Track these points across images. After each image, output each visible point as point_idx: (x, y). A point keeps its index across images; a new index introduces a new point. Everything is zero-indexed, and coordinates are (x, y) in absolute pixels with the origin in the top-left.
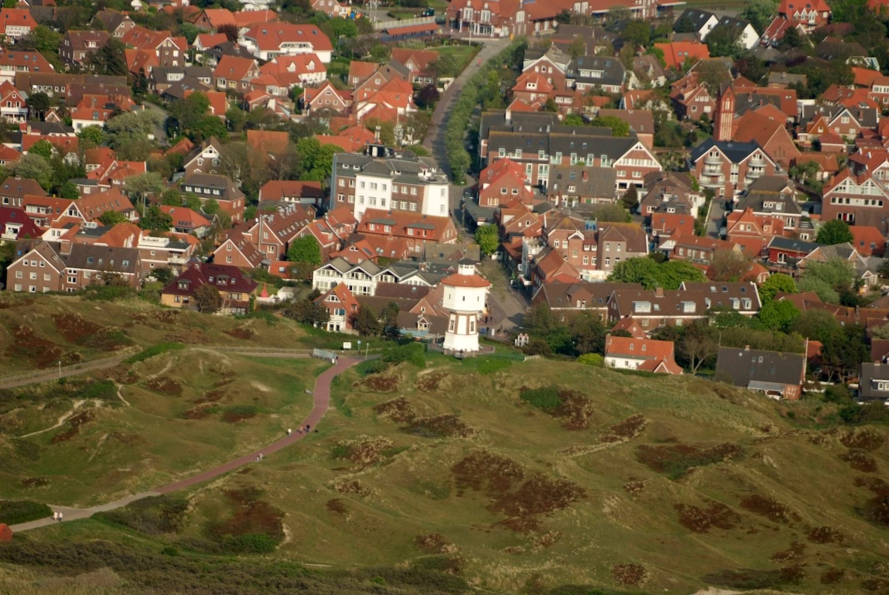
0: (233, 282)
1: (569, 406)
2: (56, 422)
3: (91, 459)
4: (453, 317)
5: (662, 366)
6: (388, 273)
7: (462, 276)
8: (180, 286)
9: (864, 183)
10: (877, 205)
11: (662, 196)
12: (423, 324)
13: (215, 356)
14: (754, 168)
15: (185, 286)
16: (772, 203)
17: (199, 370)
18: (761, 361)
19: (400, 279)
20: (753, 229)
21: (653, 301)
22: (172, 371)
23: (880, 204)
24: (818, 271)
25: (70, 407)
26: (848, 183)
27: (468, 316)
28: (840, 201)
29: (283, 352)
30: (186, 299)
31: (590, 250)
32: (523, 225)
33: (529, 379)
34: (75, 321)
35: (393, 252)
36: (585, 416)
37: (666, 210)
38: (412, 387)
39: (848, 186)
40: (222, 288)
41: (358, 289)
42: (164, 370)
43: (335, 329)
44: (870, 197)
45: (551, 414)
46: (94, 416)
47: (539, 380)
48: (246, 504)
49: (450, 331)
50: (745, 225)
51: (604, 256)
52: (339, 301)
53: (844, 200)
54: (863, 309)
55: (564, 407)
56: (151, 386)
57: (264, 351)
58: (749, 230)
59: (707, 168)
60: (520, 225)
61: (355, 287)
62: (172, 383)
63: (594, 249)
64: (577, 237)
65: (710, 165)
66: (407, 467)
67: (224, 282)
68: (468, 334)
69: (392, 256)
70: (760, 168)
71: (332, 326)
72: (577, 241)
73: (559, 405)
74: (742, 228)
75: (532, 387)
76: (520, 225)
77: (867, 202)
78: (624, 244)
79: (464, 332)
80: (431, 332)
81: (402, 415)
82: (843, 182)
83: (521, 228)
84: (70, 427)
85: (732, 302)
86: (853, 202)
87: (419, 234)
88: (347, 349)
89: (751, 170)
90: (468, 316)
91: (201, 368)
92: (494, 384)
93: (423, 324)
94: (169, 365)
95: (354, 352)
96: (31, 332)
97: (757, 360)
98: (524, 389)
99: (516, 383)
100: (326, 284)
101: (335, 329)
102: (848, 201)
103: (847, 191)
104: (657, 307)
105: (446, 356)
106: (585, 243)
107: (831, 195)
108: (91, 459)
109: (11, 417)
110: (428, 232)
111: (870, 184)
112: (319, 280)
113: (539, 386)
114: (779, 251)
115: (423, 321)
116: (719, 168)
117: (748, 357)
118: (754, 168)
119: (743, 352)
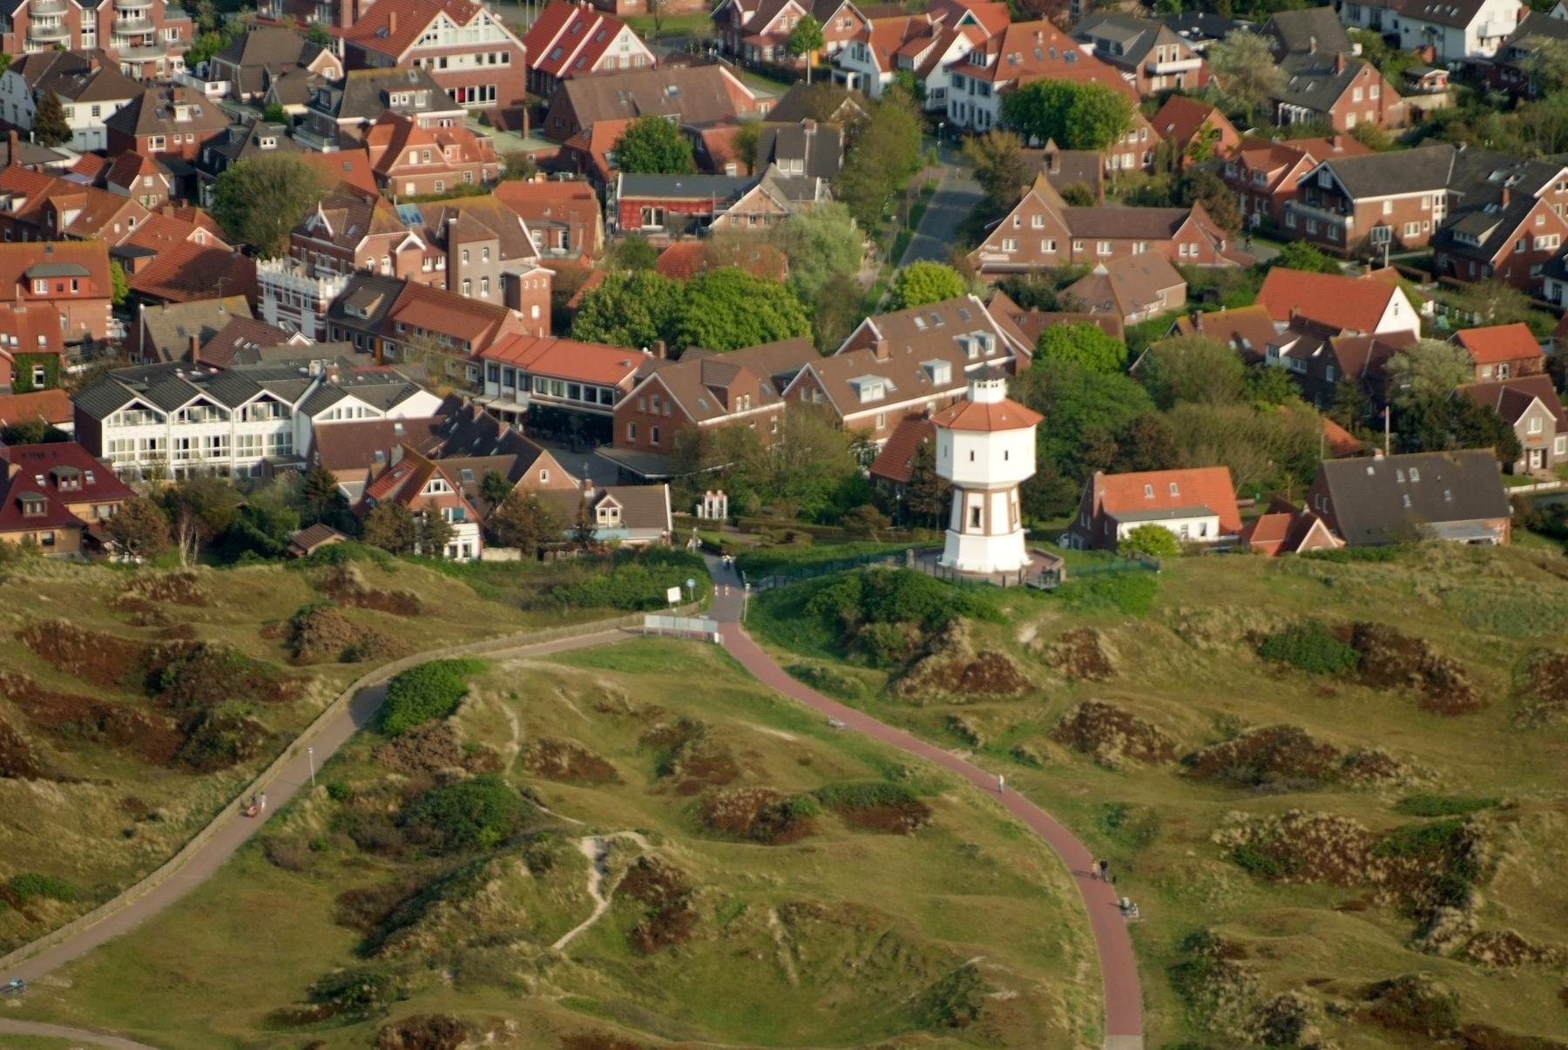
0: (90, 479)
1: (1390, 659)
2: (591, 902)
3: (793, 976)
4: (975, 500)
5: (1318, 528)
6: (265, 398)
7: (987, 406)
8: (28, 508)
9: (473, 21)
10: (499, 63)
11: (171, 111)
12: (609, 511)
13: (571, 676)
14: (125, 13)
15: (38, 507)
16: (407, 94)
17: (576, 716)
18: (1416, 479)
19: (295, 407)
20: (436, 158)
21: (881, 372)
22: (530, 727)
23: (505, 59)
24: (830, 239)
25: (583, 861)
26: (441, 24)
27: (1008, 490)
28: (492, 60)
29: (572, 634)
30: (47, 536)
31: (434, 269)
32: (123, 229)
33: (1247, 615)
34: (73, 639)
35: (42, 339)
36: (1458, 676)
37: (256, 142)
38: (1056, 676)
39: (441, 31)
40: (76, 497)
41: (201, 443)
42: (515, 725)
43: (460, 552)
44: (484, 48)
45: (1362, 683)
46: (681, 873)
47: (1269, 616)
48: (1440, 1036)
49: (969, 529)
50: (419, 152)
51: (462, 276)
52: (451, 492)
53: (486, 57)
54: (1208, 315)
55: (1383, 664)
56: (543, 769)
57: (538, 640)
58: (427, 162)
59: (36, 26)
60: (117, 228)
61: (196, 440)
62: (581, 756)
63: (441, 266)
64: (412, 246)
65: (40, 19)
66: (1527, 880)
67: (74, 483)
68: (1012, 531)
69: (43, 348)
70: (137, 13)
71: (454, 549)
72: (412, 254)
73: (1361, 663)
74: (413, 159)
75: (1266, 630)
76: (117, 228)
77: (479, 60)
78: (494, 245)
79: (1006, 529)
80: (624, 525)
81: (1151, 749)
82: (432, 24)
83: (120, 236)
84: (642, 906)
85: (965, 345)
86: (454, 64)
87: (60, 289)
88: (675, 604)
89: (120, 19)
90: (1008, 490)
91: (572, 707)
92: (1185, 636)
93: (609, 511)
94: (510, 713)
95: (693, 606)
96: (32, 683)
97: (1407, 477)
98: (1251, 637)
99: (1227, 630)
100: (132, 442)
101: (460, 552)
102: (444, 64)
103: (441, 43)
104: (889, 383)
105: (1015, 589)
106: (425, 256)
107: (413, 54)
108: (793, 976)
109: (496, 906)
110: (81, 282)
111: (482, 20)
112: (115, 439)
113: (1280, 626)
114: (642, 203)
115: (609, 504)
116: (57, 24)
117: (1386, 472)
118: (125, 13)
119: (1373, 464)
